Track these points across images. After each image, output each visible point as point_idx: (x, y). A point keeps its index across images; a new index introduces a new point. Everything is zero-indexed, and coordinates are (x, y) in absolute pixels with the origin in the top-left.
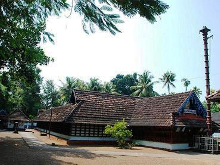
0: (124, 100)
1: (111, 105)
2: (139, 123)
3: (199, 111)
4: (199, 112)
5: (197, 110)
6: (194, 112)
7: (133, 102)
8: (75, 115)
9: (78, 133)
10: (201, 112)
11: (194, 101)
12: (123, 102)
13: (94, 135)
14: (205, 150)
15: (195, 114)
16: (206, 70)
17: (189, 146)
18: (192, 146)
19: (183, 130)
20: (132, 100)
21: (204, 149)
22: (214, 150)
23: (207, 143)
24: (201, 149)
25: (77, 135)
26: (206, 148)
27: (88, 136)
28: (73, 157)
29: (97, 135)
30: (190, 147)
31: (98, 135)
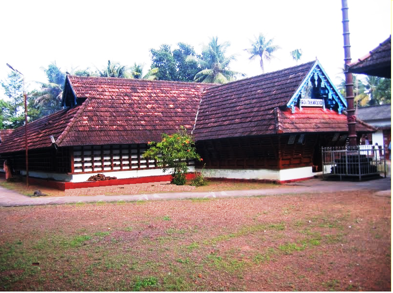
0: (177, 92)
1: (150, 104)
2: (202, 135)
3: (330, 100)
4: (329, 103)
5: (326, 99)
6: (319, 102)
7: (196, 93)
8: (280, 153)
9: (143, 164)
10: (334, 103)
11: (319, 80)
12: (175, 95)
13: (139, 166)
14: (344, 175)
15: (322, 107)
16: (347, 5)
17: (314, 171)
18: (320, 169)
19: (301, 141)
20: (193, 90)
21: (342, 173)
22: (361, 174)
23: (348, 162)
24: (338, 174)
25: (141, 167)
26: (347, 171)
27: (154, 168)
28: (190, 185)
29: (154, 166)
30: (316, 174)
31: (130, 167)
